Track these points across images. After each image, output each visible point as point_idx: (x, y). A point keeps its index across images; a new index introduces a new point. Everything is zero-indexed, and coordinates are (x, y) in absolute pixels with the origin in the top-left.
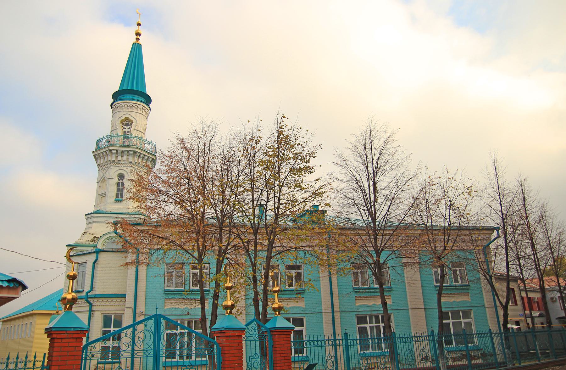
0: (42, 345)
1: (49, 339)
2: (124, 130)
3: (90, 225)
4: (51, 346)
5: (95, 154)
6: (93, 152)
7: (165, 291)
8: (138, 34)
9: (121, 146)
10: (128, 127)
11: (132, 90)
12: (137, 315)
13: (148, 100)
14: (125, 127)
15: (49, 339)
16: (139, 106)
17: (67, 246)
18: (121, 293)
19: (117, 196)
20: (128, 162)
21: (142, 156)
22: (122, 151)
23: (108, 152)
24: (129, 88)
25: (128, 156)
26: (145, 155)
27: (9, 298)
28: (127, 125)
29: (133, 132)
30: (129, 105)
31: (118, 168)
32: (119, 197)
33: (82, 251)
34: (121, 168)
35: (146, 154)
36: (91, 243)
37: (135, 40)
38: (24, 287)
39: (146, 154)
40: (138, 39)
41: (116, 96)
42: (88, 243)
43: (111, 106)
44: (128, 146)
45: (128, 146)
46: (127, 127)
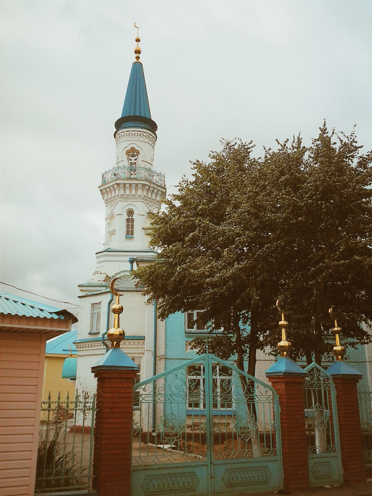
0: (89, 384)
1: (97, 378)
2: (130, 161)
3: (101, 265)
4: (100, 386)
5: (101, 188)
6: (99, 187)
7: (186, 333)
8: (138, 52)
9: (128, 179)
10: (135, 158)
11: (136, 118)
12: (157, 359)
13: (152, 126)
14: (131, 158)
15: (97, 378)
16: (145, 134)
17: (79, 286)
18: (133, 335)
19: (128, 234)
20: (137, 196)
21: (151, 189)
22: (130, 185)
23: (115, 186)
24: (132, 115)
25: (136, 190)
26: (154, 188)
27: (60, 331)
28: (133, 156)
29: (140, 163)
30: (134, 133)
31: (126, 203)
32: (130, 233)
33: (95, 291)
34: (130, 203)
35: (156, 187)
36: (104, 283)
37: (135, 60)
38: (75, 320)
39: (156, 187)
40: (138, 58)
41: (119, 124)
42: (100, 282)
43: (115, 136)
44: (136, 179)
45: (136, 179)
46: (133, 159)
